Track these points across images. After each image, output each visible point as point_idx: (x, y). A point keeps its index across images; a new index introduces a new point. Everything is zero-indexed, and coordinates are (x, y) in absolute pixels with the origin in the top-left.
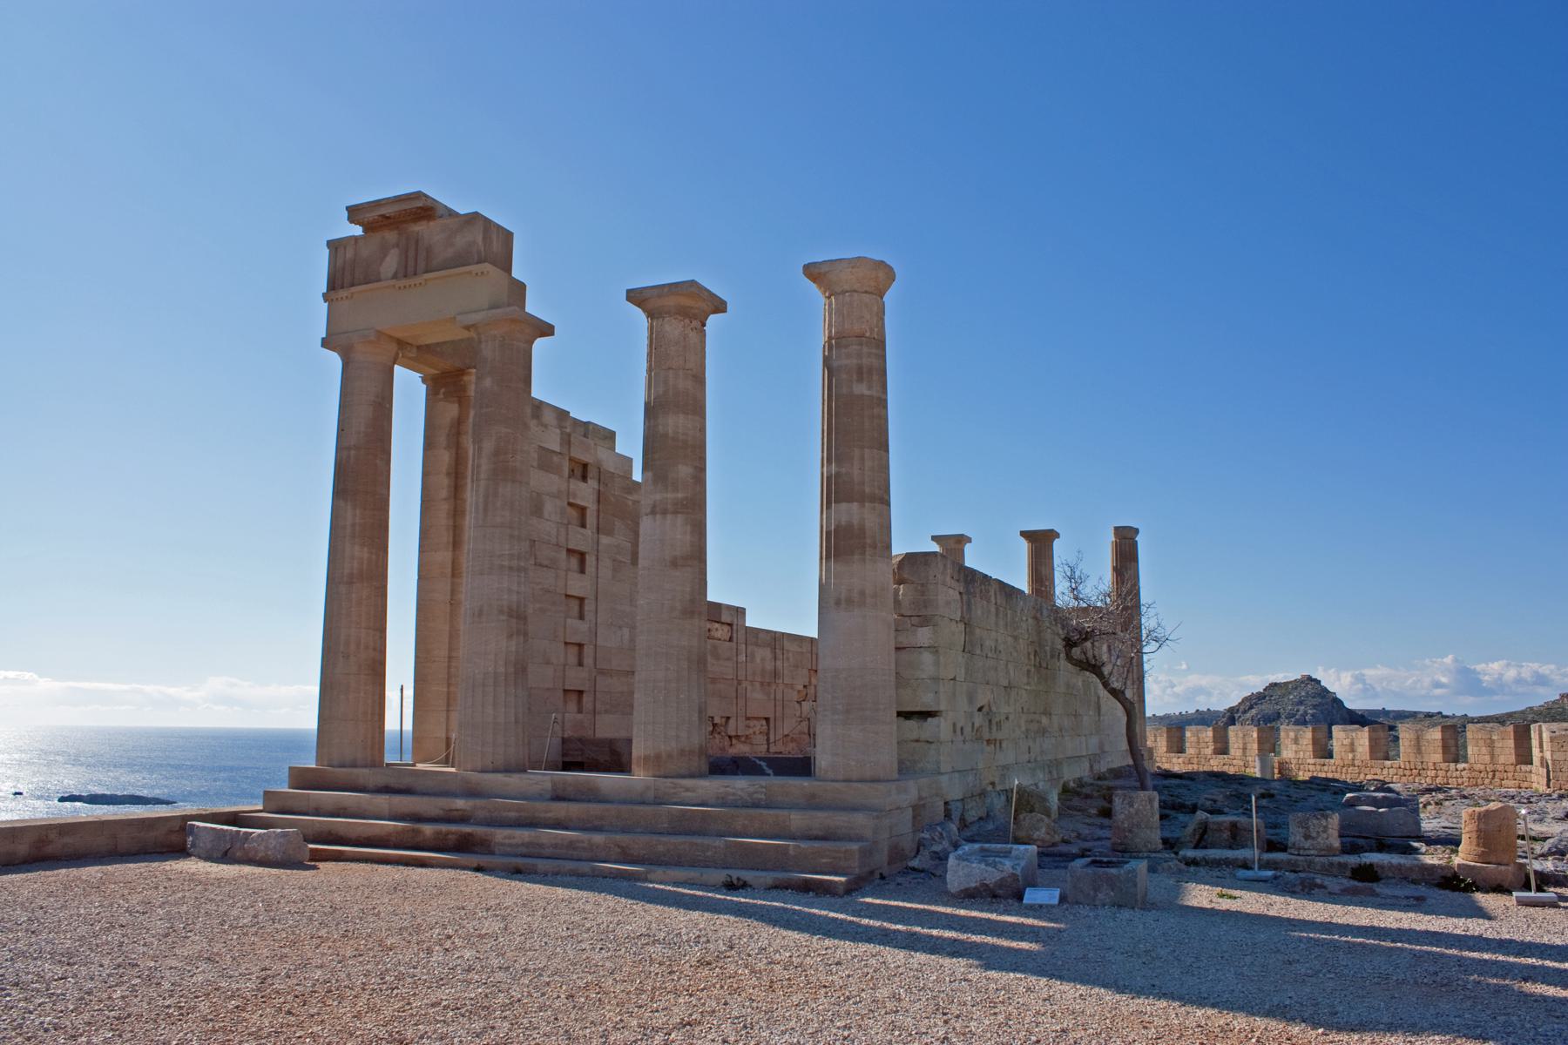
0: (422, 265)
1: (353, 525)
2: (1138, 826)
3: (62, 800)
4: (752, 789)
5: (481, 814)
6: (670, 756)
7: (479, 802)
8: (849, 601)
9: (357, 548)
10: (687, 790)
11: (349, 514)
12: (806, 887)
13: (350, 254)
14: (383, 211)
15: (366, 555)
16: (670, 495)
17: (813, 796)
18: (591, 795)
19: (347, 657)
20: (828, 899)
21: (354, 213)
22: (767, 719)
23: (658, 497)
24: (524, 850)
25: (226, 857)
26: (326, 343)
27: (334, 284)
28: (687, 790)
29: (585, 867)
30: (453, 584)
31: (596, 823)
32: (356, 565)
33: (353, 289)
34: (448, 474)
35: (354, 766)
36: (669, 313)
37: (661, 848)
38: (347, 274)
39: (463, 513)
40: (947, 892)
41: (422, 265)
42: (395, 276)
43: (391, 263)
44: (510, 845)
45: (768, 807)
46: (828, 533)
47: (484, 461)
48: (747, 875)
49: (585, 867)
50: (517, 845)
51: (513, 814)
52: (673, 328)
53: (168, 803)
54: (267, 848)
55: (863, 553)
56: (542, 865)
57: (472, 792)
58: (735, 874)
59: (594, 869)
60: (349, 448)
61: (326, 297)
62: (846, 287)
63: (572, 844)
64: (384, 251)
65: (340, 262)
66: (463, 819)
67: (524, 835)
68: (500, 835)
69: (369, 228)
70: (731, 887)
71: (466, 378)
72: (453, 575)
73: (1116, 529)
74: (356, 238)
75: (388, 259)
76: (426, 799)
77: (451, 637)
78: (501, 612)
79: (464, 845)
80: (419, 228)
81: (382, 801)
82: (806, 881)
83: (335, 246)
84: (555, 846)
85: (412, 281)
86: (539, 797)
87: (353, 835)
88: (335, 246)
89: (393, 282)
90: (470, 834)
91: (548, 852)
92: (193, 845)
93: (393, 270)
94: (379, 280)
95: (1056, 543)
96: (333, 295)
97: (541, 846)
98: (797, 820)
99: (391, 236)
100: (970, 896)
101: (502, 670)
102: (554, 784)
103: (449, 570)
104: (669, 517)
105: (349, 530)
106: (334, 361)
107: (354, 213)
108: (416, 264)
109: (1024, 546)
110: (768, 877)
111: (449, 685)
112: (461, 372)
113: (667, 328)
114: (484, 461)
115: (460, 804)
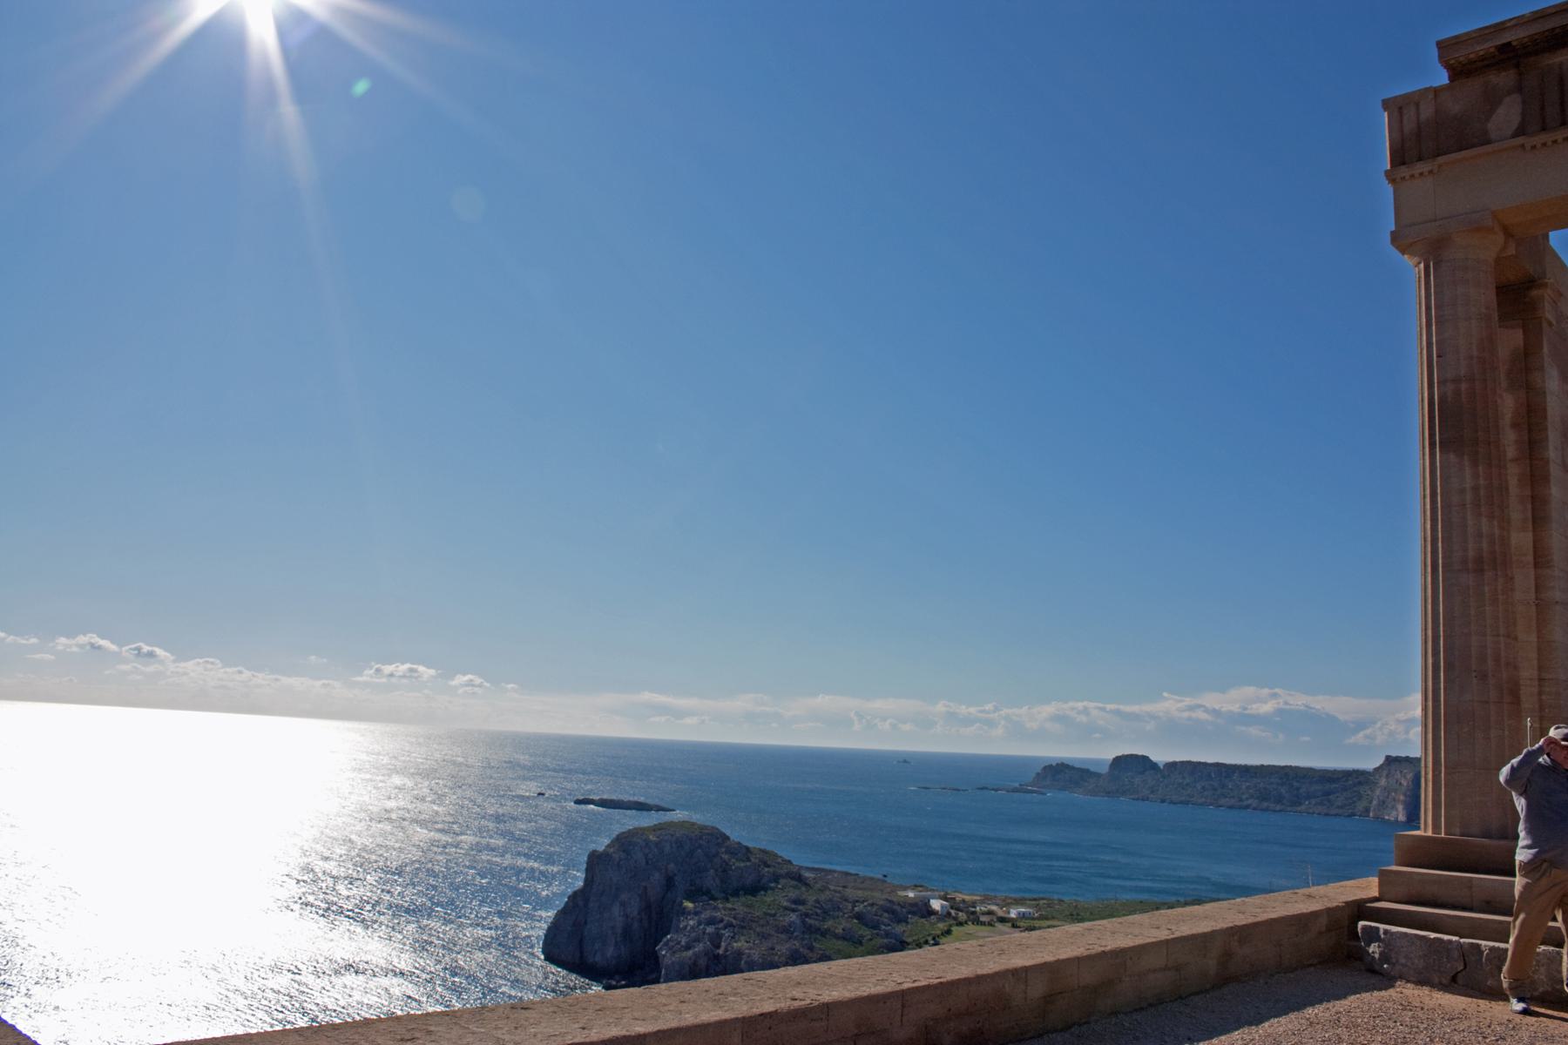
1: (1476, 489)
3: (578, 802)
9: (1484, 520)
11: (1468, 472)
13: (1427, 112)
14: (1507, 37)
15: (1497, 531)
19: (1483, 677)
26: (1396, 238)
27: (1401, 156)
30: (1536, 578)
32: (1485, 545)
33: (1441, 159)
38: (1423, 140)
39: (1546, 479)
42: (1521, 131)
43: (1508, 114)
53: (659, 809)
60: (1457, 381)
61: (1391, 177)
64: (1492, 101)
65: (1409, 125)
67: (1063, 863)
69: (1459, 72)
71: (1535, 293)
72: (1536, 565)
74: (1437, 91)
75: (1501, 110)
83: (1397, 107)
85: (1538, 139)
88: (1397, 107)
89: (1520, 140)
92: (1385, 957)
93: (1516, 121)
94: (1489, 142)
96: (1404, 171)
103: (1530, 558)
105: (1469, 497)
106: (1411, 268)
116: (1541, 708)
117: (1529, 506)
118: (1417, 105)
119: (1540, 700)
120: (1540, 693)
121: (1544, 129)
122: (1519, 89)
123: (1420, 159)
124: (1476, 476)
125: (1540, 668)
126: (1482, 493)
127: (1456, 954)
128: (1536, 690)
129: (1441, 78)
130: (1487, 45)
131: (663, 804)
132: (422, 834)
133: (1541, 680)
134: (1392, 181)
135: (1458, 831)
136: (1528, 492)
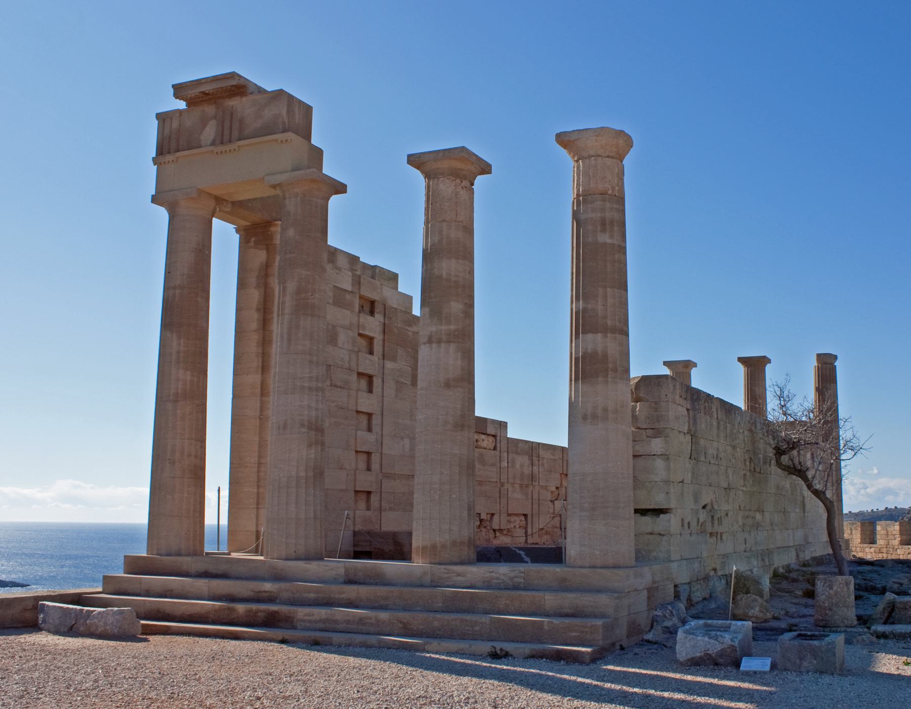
0: (235, 134)
1: (178, 352)
2: (837, 605)
4: (512, 574)
5: (285, 595)
6: (444, 546)
7: (283, 585)
8: (594, 417)
10: (459, 575)
12: (558, 657)
14: (206, 88)
16: (444, 328)
17: (564, 580)
18: (378, 579)
20: (576, 666)
21: (179, 90)
22: (525, 516)
23: (434, 329)
24: (321, 625)
25: (71, 632)
27: (163, 150)
28: (459, 575)
29: (372, 640)
31: (382, 602)
32: (180, 386)
33: (178, 154)
34: (258, 310)
35: (179, 554)
36: (443, 174)
37: (436, 624)
38: (172, 141)
39: (270, 342)
40: (676, 661)
41: (235, 134)
42: (213, 144)
43: (210, 132)
44: (310, 621)
45: (525, 589)
46: (577, 359)
47: (288, 299)
48: (509, 647)
49: (372, 640)
50: (316, 622)
51: (312, 595)
52: (446, 187)
53: (22, 586)
54: (106, 624)
55: (606, 376)
56: (336, 638)
57: (278, 577)
58: (499, 645)
59: (380, 641)
60: (174, 288)
62: (592, 153)
63: (361, 620)
66: (271, 599)
68: (302, 612)
69: (191, 103)
70: (495, 656)
71: (272, 229)
72: (262, 395)
73: (819, 355)
74: (180, 112)
75: (207, 129)
76: (239, 582)
77: (260, 446)
78: (302, 425)
79: (271, 621)
80: (233, 102)
81: (202, 584)
82: (559, 652)
83: (162, 118)
84: (348, 622)
86: (335, 581)
87: (178, 612)
88: (162, 118)
89: (212, 148)
90: (276, 612)
91: (342, 626)
92: (44, 621)
93: (212, 137)
94: (200, 147)
95: (768, 368)
97: (336, 622)
98: (550, 600)
99: (210, 110)
100: (695, 664)
102: (347, 570)
103: (258, 391)
104: (434, 345)
106: (162, 215)
107: (179, 90)
108: (231, 133)
109: (741, 369)
110: (527, 648)
111: (258, 487)
112: (268, 224)
113: (442, 187)
114: (288, 299)
115: (268, 586)
117: (260, 359)
118: (171, 119)
119: (258, 477)
120: (259, 472)
121: (222, 143)
122: (215, 118)
123: (169, 153)
124: (179, 344)
126: (181, 355)
127: (73, 615)
128: (256, 470)
129: (182, 105)
130: (195, 91)
131: (25, 583)
132: (252, 594)
135: (155, 552)
136: (260, 351)
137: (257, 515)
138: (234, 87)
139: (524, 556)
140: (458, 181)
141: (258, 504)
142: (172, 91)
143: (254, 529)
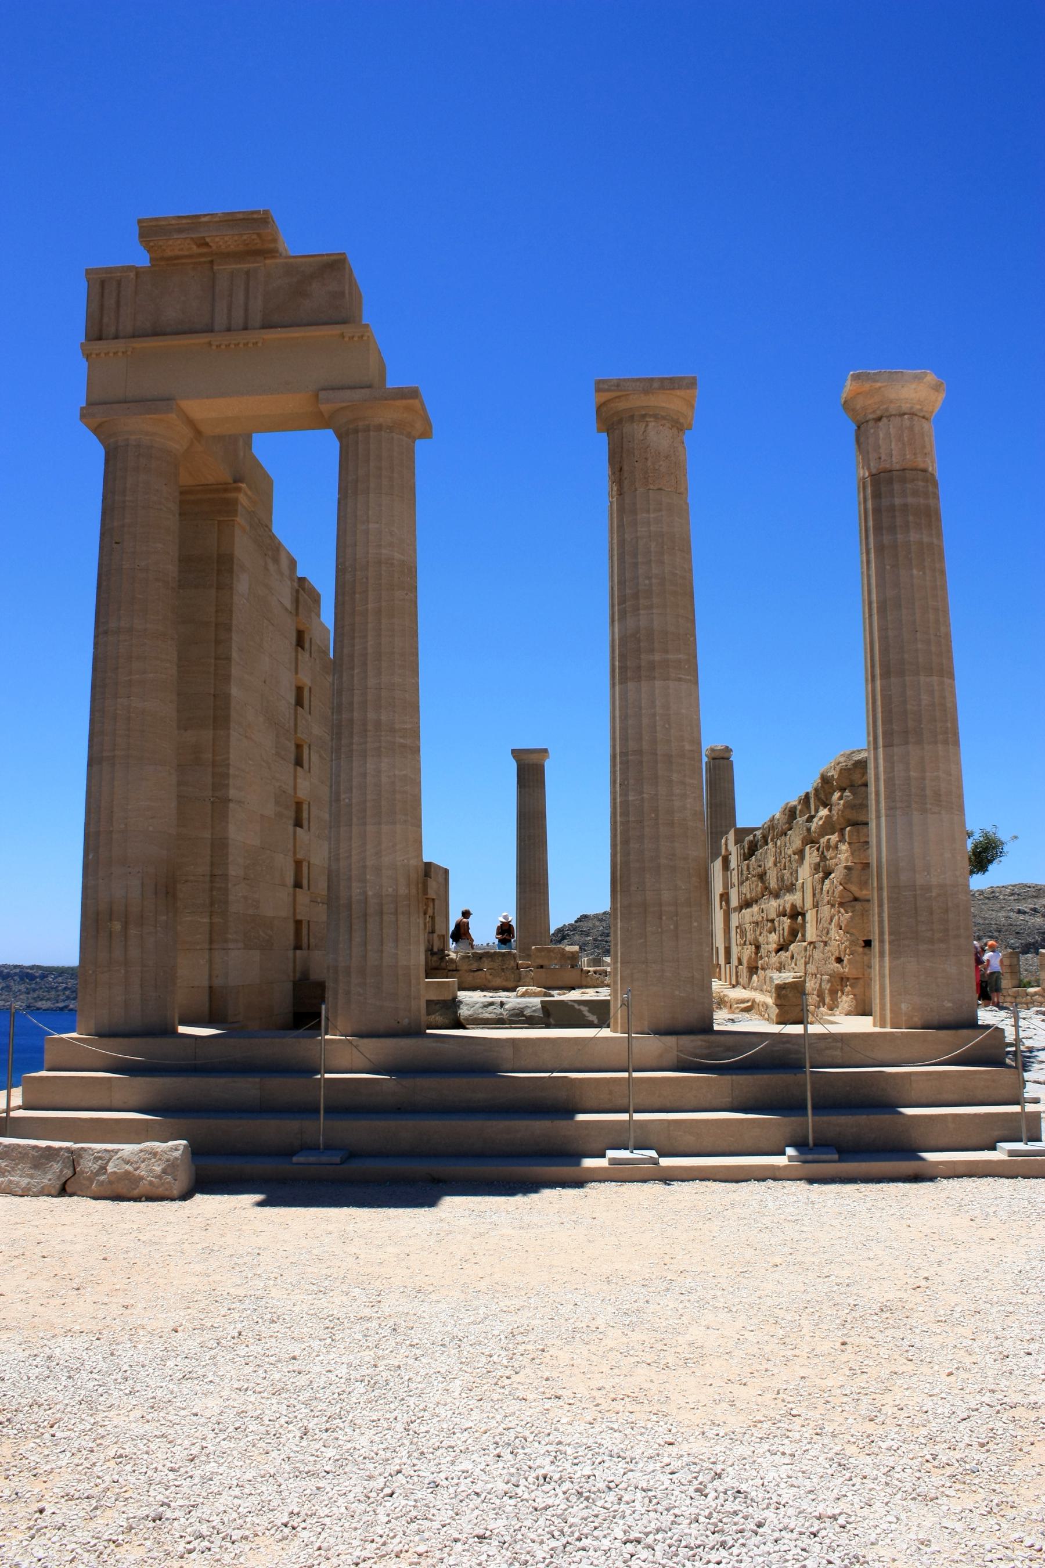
21: (150, 232)
62: (905, 407)
74: (138, 272)
101: (403, 890)
107: (150, 232)
111: (211, 914)
116: (212, 904)
120: (211, 889)
125: (212, 864)
129: (142, 259)
133: (212, 876)
134: (88, 357)
137: (211, 962)
138: (254, 230)
139: (587, 1014)
140: (675, 430)
141: (211, 942)
142: (136, 229)
143: (206, 983)
